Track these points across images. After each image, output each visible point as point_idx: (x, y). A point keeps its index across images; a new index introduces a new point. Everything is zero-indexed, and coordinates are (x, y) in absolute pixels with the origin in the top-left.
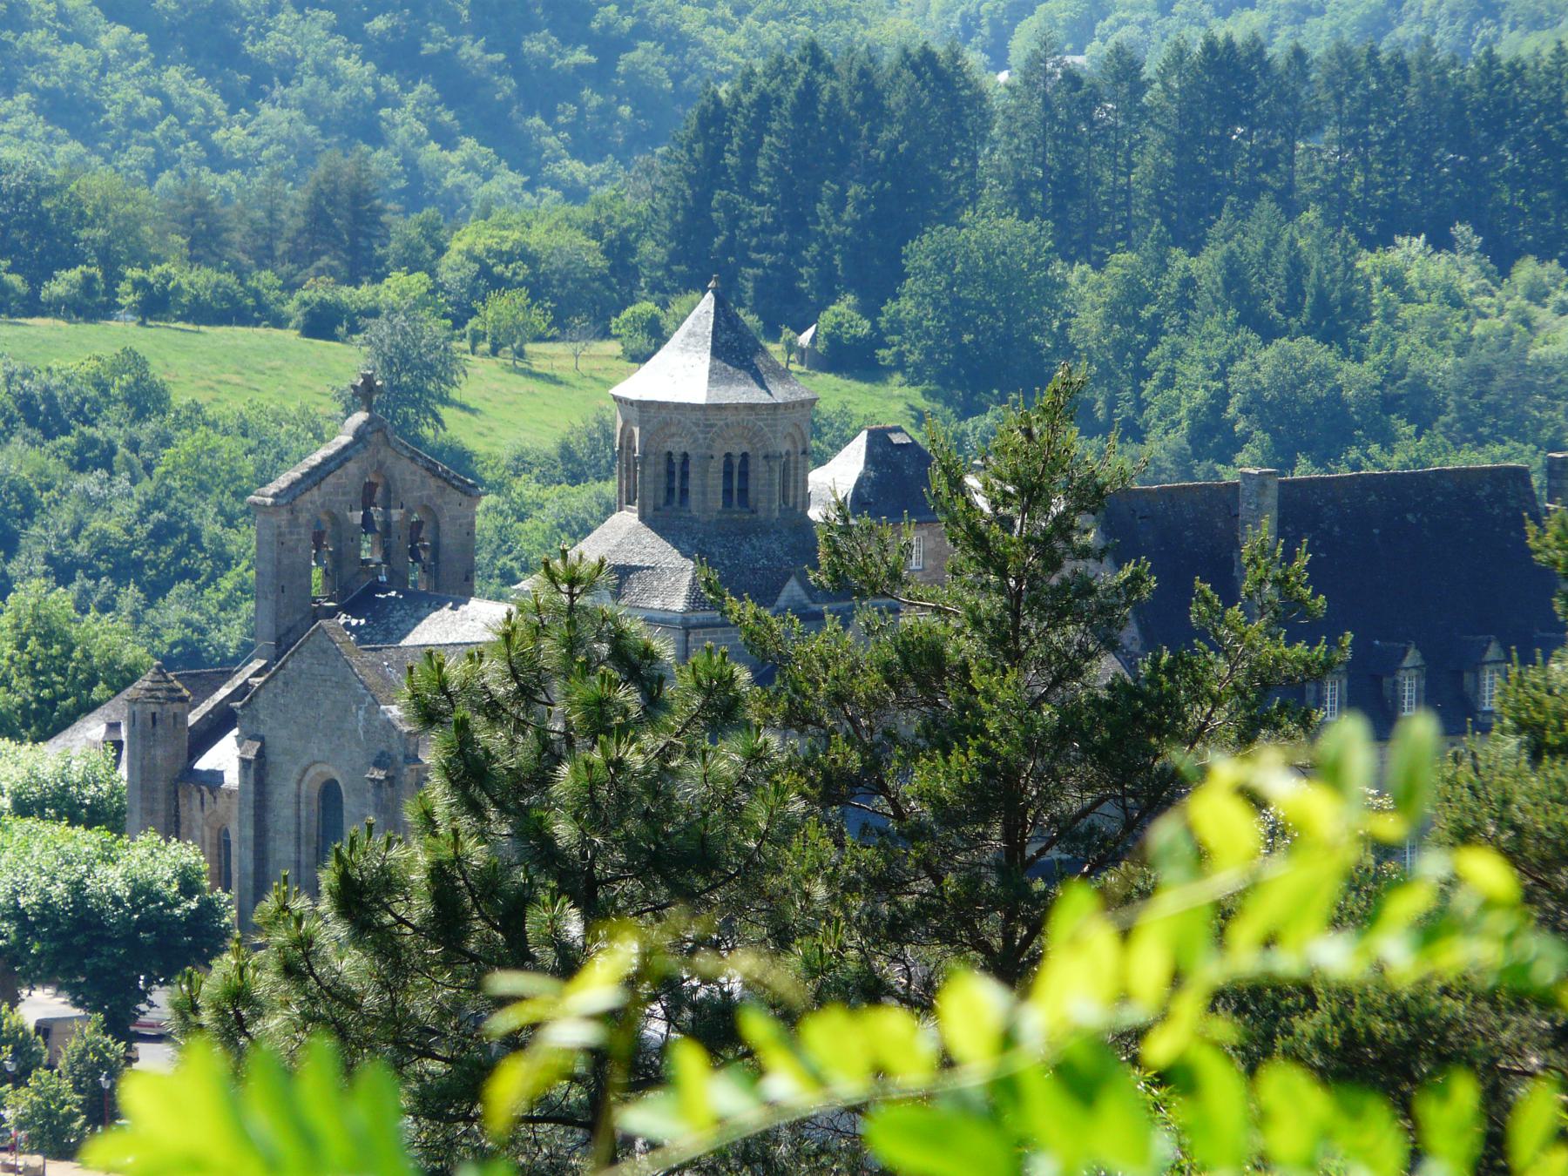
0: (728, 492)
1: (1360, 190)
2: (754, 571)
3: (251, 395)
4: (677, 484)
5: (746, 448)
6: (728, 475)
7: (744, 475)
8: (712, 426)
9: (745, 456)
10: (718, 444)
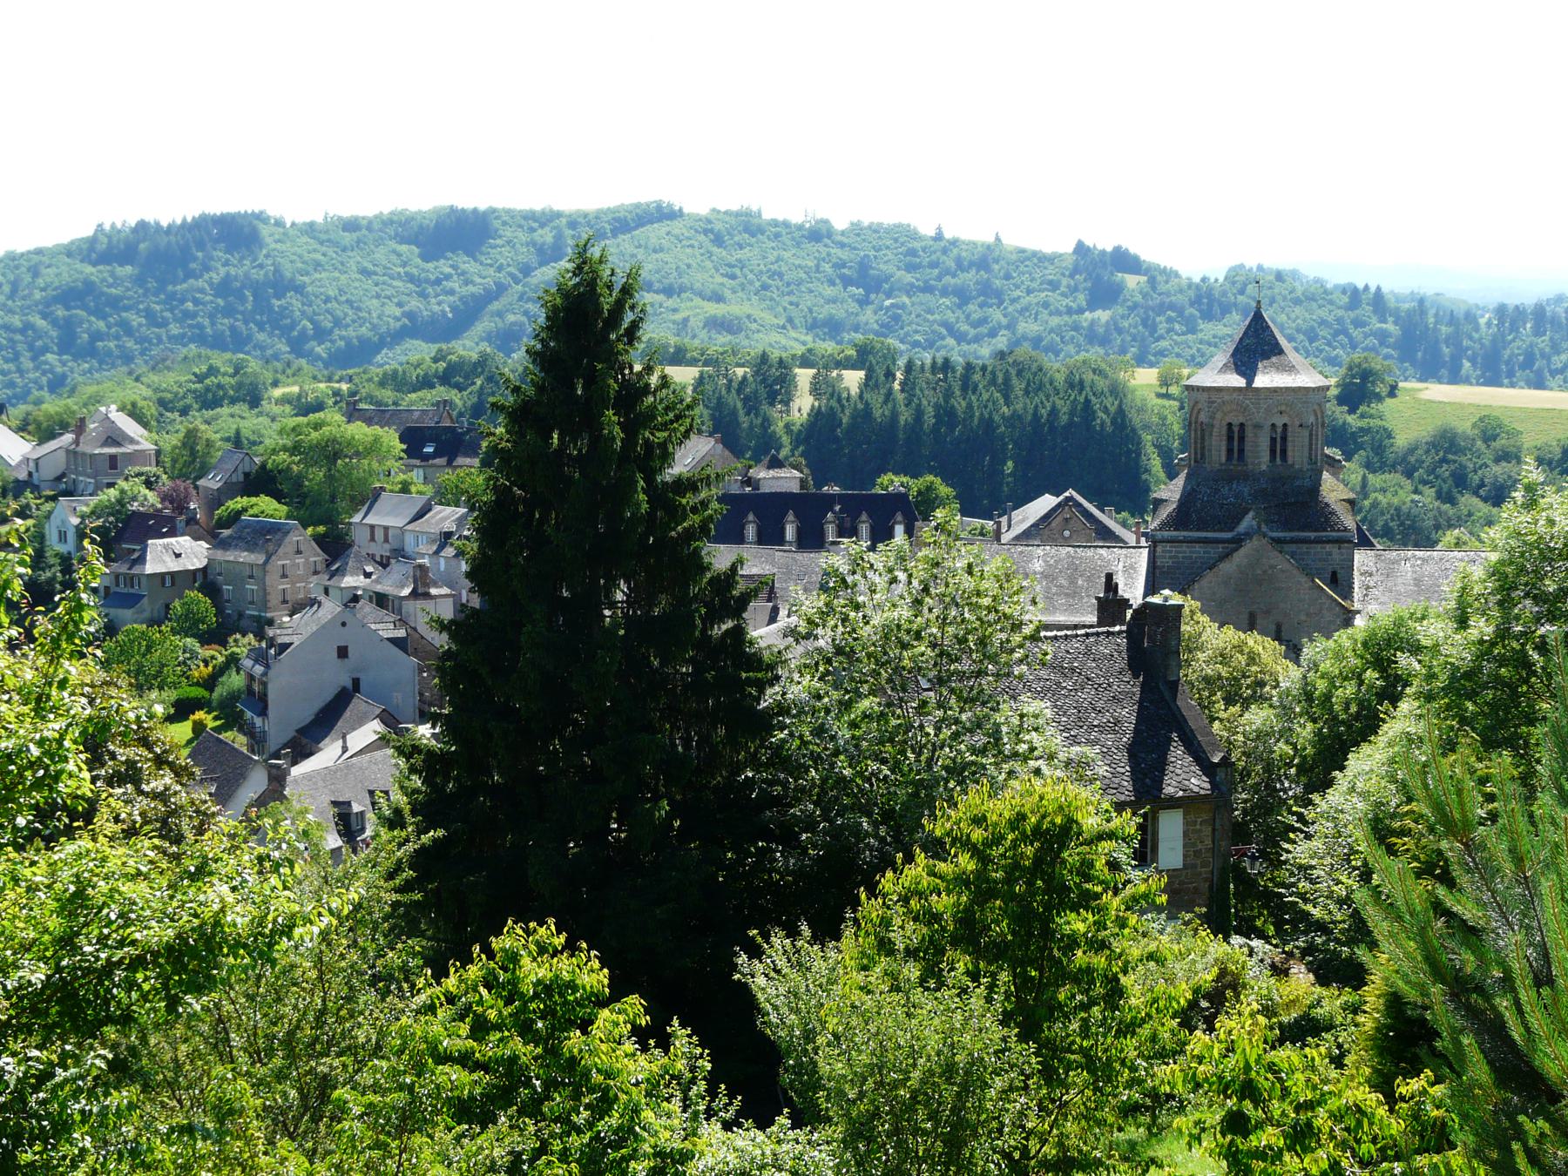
0: (1230, 451)
1: (260, 641)
2: (1222, 506)
3: (1438, 758)
4: (1236, 443)
5: (1242, 420)
6: (1230, 438)
7: (1242, 439)
8: (1213, 402)
9: (1242, 425)
10: (1219, 416)
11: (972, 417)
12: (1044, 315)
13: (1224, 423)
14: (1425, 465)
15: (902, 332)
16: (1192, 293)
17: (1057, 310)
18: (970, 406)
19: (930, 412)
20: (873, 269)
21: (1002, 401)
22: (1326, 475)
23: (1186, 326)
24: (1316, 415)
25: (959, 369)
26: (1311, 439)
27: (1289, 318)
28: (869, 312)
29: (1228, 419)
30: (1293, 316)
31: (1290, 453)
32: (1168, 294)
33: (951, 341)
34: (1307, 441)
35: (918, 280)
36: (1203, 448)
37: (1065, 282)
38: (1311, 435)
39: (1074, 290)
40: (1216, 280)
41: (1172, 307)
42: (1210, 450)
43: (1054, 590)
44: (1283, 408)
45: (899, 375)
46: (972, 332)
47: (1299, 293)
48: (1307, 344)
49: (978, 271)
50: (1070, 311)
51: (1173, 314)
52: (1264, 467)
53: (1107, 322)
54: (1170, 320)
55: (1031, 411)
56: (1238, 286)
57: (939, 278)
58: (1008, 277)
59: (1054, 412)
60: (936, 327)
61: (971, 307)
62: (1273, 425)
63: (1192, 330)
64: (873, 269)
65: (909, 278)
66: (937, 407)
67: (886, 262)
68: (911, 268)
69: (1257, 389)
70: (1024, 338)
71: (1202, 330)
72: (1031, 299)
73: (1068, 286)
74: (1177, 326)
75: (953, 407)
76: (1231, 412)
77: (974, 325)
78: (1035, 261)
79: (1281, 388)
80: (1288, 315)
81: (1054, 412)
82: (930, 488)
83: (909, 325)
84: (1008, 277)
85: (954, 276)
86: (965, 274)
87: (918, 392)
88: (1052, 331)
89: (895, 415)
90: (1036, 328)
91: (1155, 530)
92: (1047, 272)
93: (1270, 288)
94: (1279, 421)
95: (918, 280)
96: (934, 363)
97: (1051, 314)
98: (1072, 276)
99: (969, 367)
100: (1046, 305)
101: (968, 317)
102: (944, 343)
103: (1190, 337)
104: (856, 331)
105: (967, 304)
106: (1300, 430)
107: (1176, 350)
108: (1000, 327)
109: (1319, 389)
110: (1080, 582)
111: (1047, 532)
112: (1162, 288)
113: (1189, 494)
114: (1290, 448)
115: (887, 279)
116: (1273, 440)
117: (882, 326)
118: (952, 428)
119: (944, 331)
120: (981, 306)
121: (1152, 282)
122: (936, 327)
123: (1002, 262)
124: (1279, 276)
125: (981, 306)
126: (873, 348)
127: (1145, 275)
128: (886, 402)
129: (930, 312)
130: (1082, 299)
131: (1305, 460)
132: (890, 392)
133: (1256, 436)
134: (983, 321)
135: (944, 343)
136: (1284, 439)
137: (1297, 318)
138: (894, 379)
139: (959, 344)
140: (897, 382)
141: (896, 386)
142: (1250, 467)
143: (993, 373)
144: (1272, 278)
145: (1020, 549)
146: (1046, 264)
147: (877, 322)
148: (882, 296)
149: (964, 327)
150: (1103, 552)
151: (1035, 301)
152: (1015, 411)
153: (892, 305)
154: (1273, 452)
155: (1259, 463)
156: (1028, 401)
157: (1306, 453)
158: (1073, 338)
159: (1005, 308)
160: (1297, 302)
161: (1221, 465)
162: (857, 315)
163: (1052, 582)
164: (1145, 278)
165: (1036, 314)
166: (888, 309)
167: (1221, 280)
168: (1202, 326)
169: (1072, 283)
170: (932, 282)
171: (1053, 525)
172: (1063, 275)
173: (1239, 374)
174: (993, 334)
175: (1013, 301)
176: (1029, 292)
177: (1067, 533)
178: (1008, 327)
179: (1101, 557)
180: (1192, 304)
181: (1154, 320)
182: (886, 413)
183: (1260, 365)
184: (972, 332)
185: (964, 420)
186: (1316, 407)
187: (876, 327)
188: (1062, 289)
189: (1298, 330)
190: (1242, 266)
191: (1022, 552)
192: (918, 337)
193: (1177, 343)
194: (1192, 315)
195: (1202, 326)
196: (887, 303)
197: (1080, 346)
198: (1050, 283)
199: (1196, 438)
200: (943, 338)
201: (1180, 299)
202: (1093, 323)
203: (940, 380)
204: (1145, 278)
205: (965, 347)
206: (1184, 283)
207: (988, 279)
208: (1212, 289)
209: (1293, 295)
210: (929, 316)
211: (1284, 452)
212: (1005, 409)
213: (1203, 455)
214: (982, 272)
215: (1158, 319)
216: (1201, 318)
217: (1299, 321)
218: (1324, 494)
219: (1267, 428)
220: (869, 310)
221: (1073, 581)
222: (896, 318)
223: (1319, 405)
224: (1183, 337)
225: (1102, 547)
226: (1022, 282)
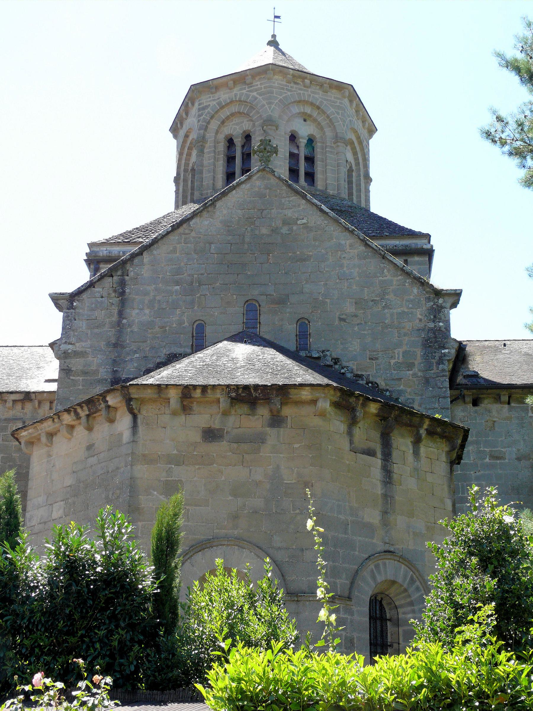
5: (246, 126)
13: (221, 137)
29: (227, 130)
136: (310, 160)
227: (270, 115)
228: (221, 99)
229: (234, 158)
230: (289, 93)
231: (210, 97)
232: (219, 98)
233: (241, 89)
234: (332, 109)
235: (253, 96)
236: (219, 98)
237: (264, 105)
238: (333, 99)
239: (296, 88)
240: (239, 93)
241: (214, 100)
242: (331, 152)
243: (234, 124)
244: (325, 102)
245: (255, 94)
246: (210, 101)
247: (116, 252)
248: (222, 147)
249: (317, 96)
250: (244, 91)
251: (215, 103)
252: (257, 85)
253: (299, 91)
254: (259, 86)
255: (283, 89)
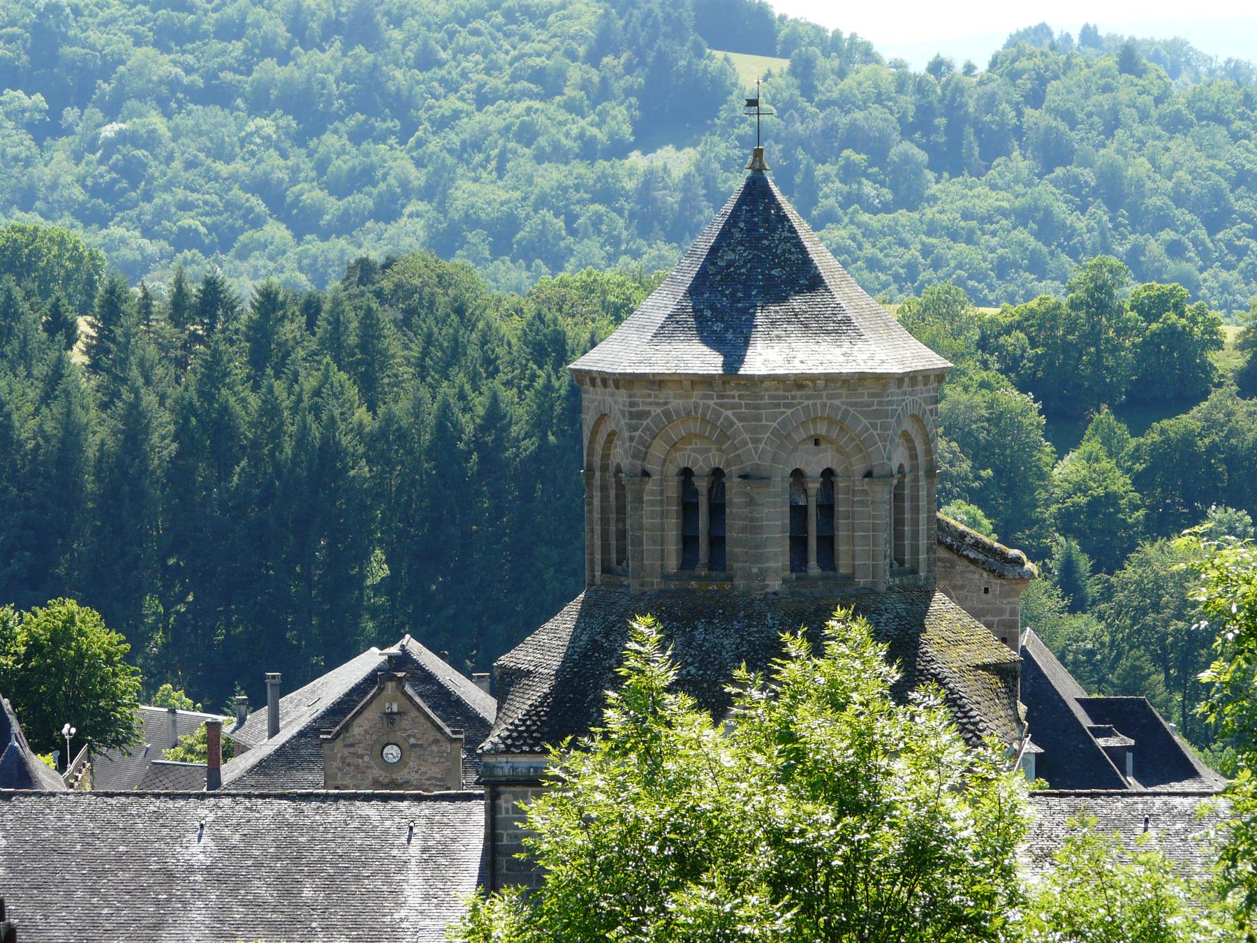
0: (688, 542)
5: (716, 460)
6: (688, 509)
7: (718, 510)
8: (641, 415)
9: (717, 474)
10: (658, 449)
11: (276, 435)
12: (523, 161)
13: (672, 469)
14: (128, 682)
15: (147, 207)
16: (908, 102)
17: (556, 146)
18: (270, 410)
19: (162, 424)
20: (73, 42)
21: (353, 392)
22: (940, 601)
23: (894, 187)
24: (912, 449)
25: (247, 311)
26: (898, 510)
27: (1157, 168)
28: (59, 156)
29: (683, 459)
30: (1166, 160)
31: (842, 548)
32: (845, 103)
33: (276, 231)
34: (885, 514)
35: (189, 70)
36: (622, 535)
37: (575, 73)
38: (898, 498)
39: (602, 93)
40: (969, 69)
41: (855, 139)
42: (638, 542)
43: (238, 913)
44: (822, 429)
45: (84, 326)
46: (333, 206)
47: (1181, 105)
48: (1202, 234)
49: (347, 47)
50: (589, 151)
51: (859, 158)
52: (775, 584)
53: (687, 177)
54: (849, 173)
55: (431, 420)
56: (1025, 83)
57: (246, 67)
58: (426, 61)
59: (495, 418)
60: (237, 193)
61: (331, 142)
62: (798, 474)
63: (909, 198)
64: (73, 42)
65: (164, 65)
66: (184, 411)
67: (105, 24)
68: (168, 38)
69: (750, 378)
70: (471, 220)
71: (934, 199)
72: (490, 118)
73: (585, 86)
74: (868, 188)
75: (225, 410)
76: (688, 438)
77: (340, 188)
78: (499, 19)
79: (813, 378)
80: (1152, 160)
81: (495, 418)
82: (62, 636)
83: (167, 188)
84: (426, 61)
85: (284, 58)
86: (315, 54)
87: (135, 372)
88: (542, 201)
89: (71, 435)
90: (504, 196)
91: (495, 751)
92: (528, 48)
93: (1107, 89)
94: (814, 463)
95: (189, 70)
96: (180, 294)
97: (540, 158)
98: (593, 59)
99: (269, 302)
100: (526, 134)
101: (321, 167)
102: (258, 235)
103: (903, 216)
104: (26, 207)
105: (319, 132)
106: (866, 484)
107: (869, 250)
108: (407, 192)
109: (913, 378)
110: (307, 893)
111: (339, 748)
112: (829, 88)
113: (584, 656)
114: (842, 533)
115: (109, 66)
116: (798, 513)
117: (95, 191)
118: (224, 467)
119: (259, 205)
120: (357, 137)
121: (804, 72)
122: (237, 193)
123: (412, 24)
124: (1129, 59)
125: (357, 137)
126: (37, 254)
127: (785, 55)
128: (46, 399)
129: (221, 153)
130: (620, 118)
131: (884, 564)
132: (58, 372)
133: (751, 503)
134: (363, 177)
135: (258, 235)
136: (827, 509)
137: (1176, 166)
138: (71, 340)
139: (299, 237)
140: (80, 345)
141: (78, 357)
142: (740, 583)
143: (337, 323)
144: (1110, 62)
145: (154, 805)
146: (528, 27)
147: (81, 181)
148: (96, 114)
149: (312, 194)
150: (370, 810)
151: (499, 123)
152: (389, 419)
153: (122, 137)
154: (798, 543)
155: (763, 574)
156: (425, 393)
157: (888, 550)
158: (597, 221)
159: (420, 144)
160: (1175, 124)
161: (666, 577)
162: (28, 162)
163: (233, 892)
164: (785, 64)
165: (503, 158)
166: (110, 146)
167: (982, 67)
168: (934, 189)
169: (595, 76)
170: (228, 76)
171: (356, 730)
172: (572, 55)
173: (706, 341)
174: (387, 211)
175: (442, 124)
176: (482, 100)
177: (392, 753)
178: (427, 193)
179: (365, 824)
180: (907, 131)
181: (809, 172)
182: (49, 427)
183: (760, 318)
184: (333, 206)
185: (256, 444)
186: (908, 425)
187: (78, 193)
188: (570, 92)
189: (1179, 198)
190: (1042, 31)
191: (157, 815)
192: (188, 221)
193: (869, 233)
194: (906, 159)
195: (934, 189)
196: (109, 131)
197: (616, 242)
198: (538, 76)
199: (604, 510)
200: (257, 223)
201: (876, 118)
202: (650, 181)
203: (195, 338)
204: (785, 64)
205: (314, 245)
206: (887, 76)
207: (375, 67)
208: (959, 90)
209: (1165, 108)
210: (219, 166)
211: (827, 543)
212: (361, 414)
213: (622, 551)
214: (359, 50)
215: (820, 170)
216: (931, 166)
217: (1181, 174)
218: (931, 651)
219: (781, 480)
220: (60, 150)
221: (288, 890)
222: (132, 172)
223: (917, 419)
224: (886, 218)
225: (367, 798)
226: (464, 75)
227: (758, 465)
228: (669, 406)
229: (696, 506)
230: (789, 412)
231: (650, 396)
232: (666, 403)
233: (705, 397)
234: (866, 421)
235: (727, 418)
236: (666, 403)
237: (746, 443)
238: (866, 399)
239: (801, 397)
240: (701, 402)
241: (658, 404)
242: (862, 502)
243: (693, 450)
244: (852, 410)
245: (729, 413)
246: (651, 404)
247: (524, 771)
248: (673, 489)
249: (837, 402)
250: (711, 402)
251: (659, 410)
252: (733, 397)
253: (806, 402)
254: (737, 400)
255: (778, 406)
